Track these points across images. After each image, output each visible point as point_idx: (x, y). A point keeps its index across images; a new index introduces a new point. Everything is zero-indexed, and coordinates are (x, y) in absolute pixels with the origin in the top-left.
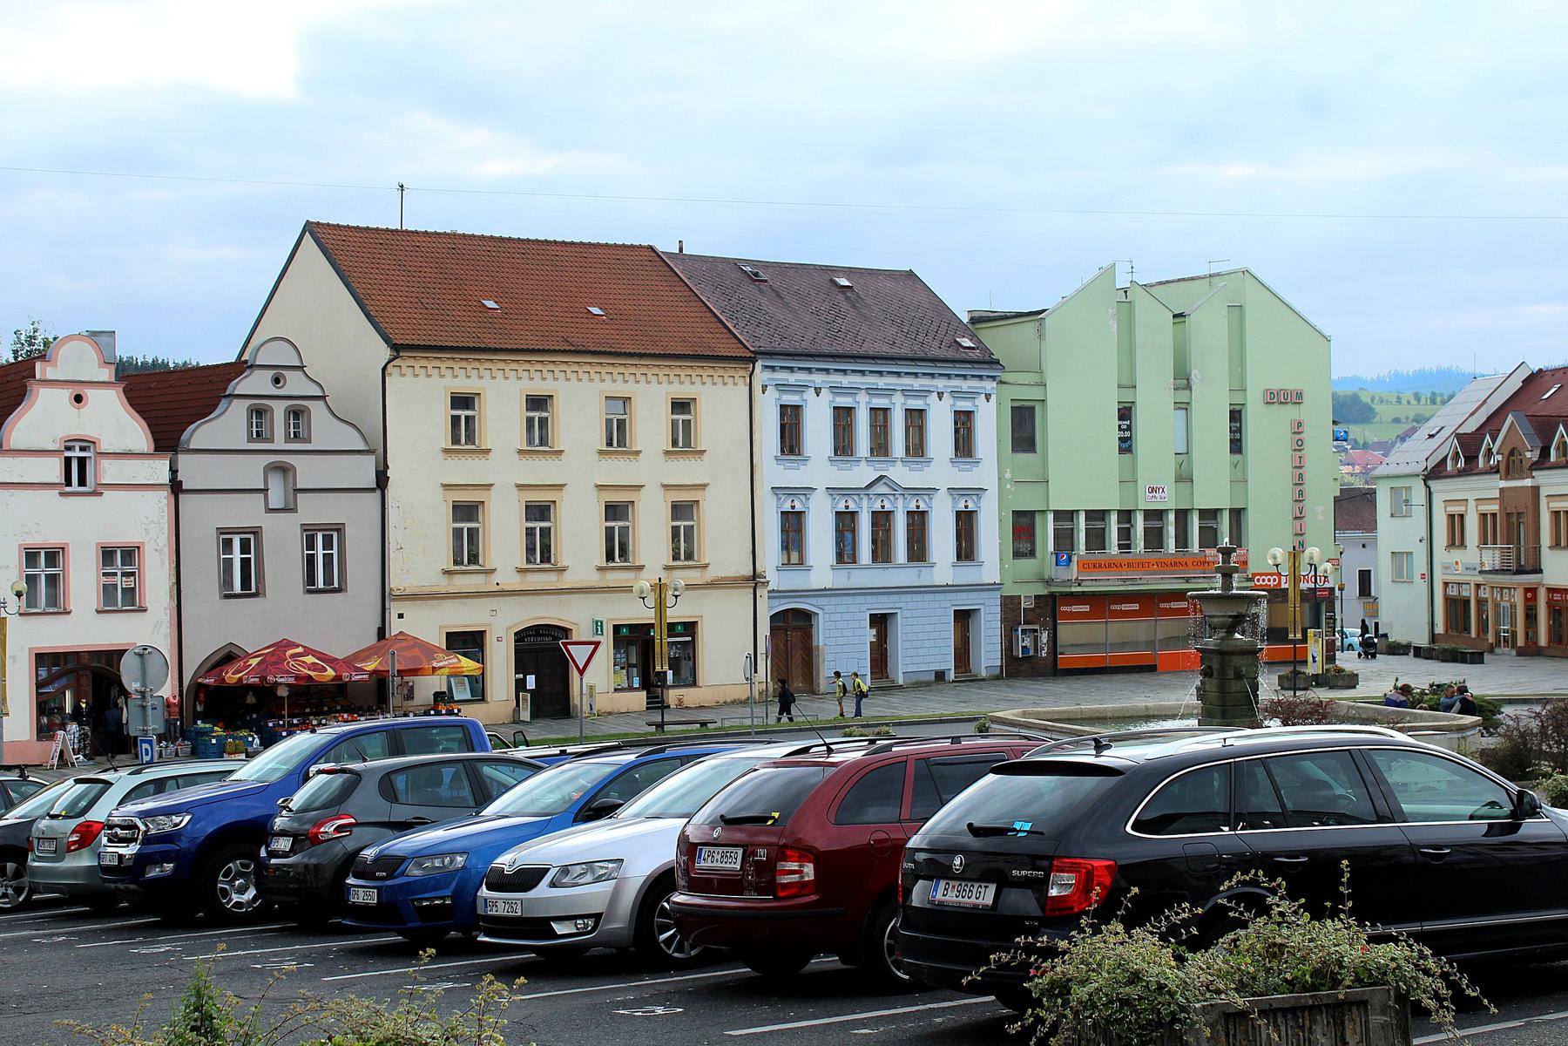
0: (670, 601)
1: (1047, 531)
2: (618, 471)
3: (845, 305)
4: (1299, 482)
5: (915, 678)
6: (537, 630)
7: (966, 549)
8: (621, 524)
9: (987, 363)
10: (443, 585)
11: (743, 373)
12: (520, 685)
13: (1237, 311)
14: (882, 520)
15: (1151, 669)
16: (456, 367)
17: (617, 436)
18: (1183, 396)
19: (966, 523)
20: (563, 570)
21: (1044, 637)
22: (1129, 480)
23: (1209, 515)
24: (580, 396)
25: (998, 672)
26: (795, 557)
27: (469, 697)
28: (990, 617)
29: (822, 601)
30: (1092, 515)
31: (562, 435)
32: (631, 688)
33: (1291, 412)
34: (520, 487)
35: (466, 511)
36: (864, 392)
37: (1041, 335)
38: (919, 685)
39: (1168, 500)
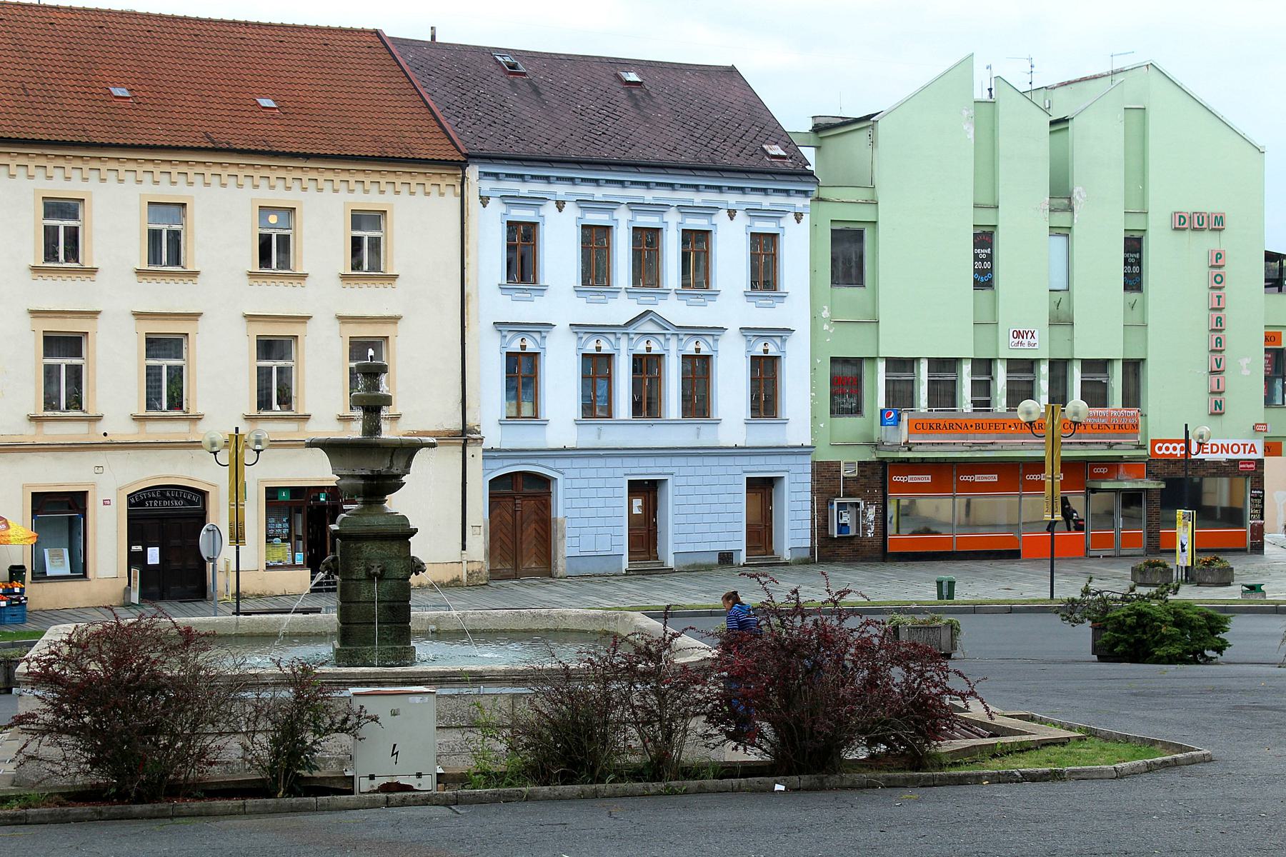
0: (249, 456)
1: (877, 384)
2: (276, 298)
3: (626, 104)
4: (1218, 327)
5: (691, 560)
6: (163, 492)
7: (765, 399)
8: (281, 363)
9: (793, 173)
10: (30, 434)
11: (450, 181)
12: (136, 560)
13: (1138, 114)
14: (646, 366)
15: (1013, 555)
16: (50, 165)
17: (273, 252)
18: (1062, 219)
19: (765, 374)
20: (197, 418)
21: (871, 513)
22: (986, 323)
23: (1097, 366)
24: (221, 210)
25: (807, 554)
26: (527, 409)
27: (68, 572)
28: (797, 487)
29: (560, 463)
30: (939, 364)
31: (92, 250)
32: (293, 566)
33: (1208, 241)
34: (139, 315)
35: (64, 344)
36: (624, 208)
37: (873, 143)
38: (694, 569)
39: (1040, 348)
